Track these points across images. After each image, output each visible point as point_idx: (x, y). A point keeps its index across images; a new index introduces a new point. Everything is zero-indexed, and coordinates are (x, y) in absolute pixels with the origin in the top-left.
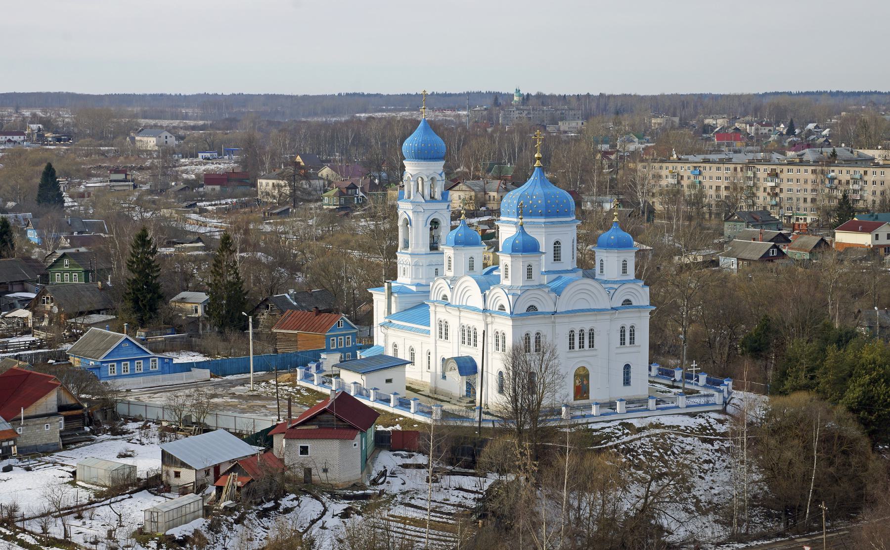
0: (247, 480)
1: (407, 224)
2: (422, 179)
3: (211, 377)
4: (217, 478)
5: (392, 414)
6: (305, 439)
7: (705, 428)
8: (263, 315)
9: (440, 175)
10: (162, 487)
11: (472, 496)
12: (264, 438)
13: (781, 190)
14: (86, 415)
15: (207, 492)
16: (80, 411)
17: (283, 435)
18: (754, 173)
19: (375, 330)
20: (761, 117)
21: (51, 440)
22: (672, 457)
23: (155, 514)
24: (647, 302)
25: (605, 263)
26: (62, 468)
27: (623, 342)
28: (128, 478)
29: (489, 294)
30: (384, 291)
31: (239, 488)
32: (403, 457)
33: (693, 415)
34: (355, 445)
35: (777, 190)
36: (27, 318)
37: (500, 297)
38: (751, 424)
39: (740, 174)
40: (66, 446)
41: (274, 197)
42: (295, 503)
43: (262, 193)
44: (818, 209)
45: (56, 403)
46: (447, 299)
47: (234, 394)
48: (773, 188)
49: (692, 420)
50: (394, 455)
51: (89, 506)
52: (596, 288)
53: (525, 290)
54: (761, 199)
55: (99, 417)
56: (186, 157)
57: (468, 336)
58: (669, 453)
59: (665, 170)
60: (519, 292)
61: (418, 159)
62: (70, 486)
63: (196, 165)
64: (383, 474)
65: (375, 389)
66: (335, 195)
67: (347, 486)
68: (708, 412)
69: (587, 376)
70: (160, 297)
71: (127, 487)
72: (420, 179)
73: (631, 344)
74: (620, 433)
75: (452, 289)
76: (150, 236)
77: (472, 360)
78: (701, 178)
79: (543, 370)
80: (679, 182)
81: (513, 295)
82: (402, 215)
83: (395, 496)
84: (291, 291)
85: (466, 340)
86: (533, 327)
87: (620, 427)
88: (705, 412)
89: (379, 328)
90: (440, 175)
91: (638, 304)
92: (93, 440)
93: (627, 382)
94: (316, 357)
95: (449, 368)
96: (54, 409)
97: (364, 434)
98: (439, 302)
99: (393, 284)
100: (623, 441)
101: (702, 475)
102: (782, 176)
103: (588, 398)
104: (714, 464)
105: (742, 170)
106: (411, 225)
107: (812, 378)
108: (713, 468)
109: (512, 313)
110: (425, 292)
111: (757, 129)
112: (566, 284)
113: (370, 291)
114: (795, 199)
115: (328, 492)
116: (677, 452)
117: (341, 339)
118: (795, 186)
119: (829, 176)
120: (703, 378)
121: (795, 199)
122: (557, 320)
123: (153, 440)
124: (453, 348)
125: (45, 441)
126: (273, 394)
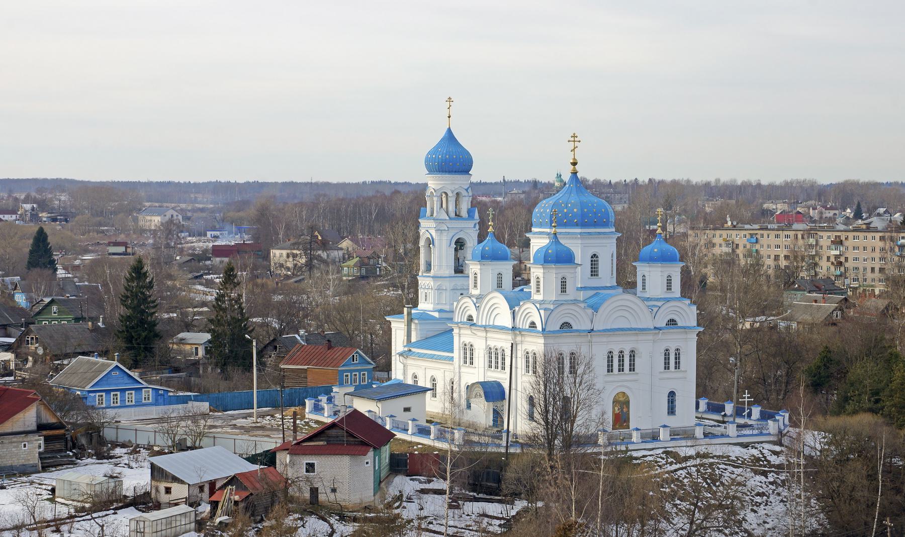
0: (245, 494)
1: (430, 244)
2: (446, 193)
3: (211, 411)
4: (212, 492)
5: (411, 442)
6: (312, 454)
7: (758, 460)
8: (270, 357)
9: (467, 190)
10: (150, 505)
11: (498, 522)
12: (269, 458)
13: (846, 259)
14: (69, 439)
15: (200, 509)
16: (62, 431)
17: (287, 452)
18: (817, 241)
19: (393, 358)
20: (825, 202)
21: (29, 460)
22: (721, 488)
23: (142, 524)
24: (694, 323)
25: (647, 278)
26: (40, 486)
27: (667, 367)
28: (112, 493)
29: (519, 310)
30: (403, 318)
31: (236, 503)
32: (421, 482)
33: (745, 446)
34: (367, 463)
35: (842, 259)
36: (9, 361)
37: (532, 313)
38: (809, 458)
39: (800, 242)
40: (45, 468)
41: (288, 269)
42: (300, 523)
43: (275, 264)
44: (887, 279)
45: (35, 419)
46: (472, 320)
47: (235, 425)
48: (837, 257)
49: (744, 450)
50: (411, 480)
51: (68, 521)
52: (636, 304)
53: (558, 304)
54: (825, 268)
55: (83, 441)
56: (194, 236)
57: (495, 358)
58: (717, 484)
59: (719, 237)
60: (552, 307)
61: (442, 172)
62: (47, 502)
63: (204, 242)
64: (399, 498)
65: (392, 416)
66: (355, 265)
67: (358, 508)
68: (762, 442)
69: (627, 403)
70: (157, 335)
71: (112, 503)
72: (444, 195)
73: (676, 368)
74: (664, 462)
75: (477, 308)
76: (145, 269)
77: (499, 385)
78: (758, 247)
79: (577, 385)
80: (733, 251)
81: (545, 310)
82: (424, 233)
83: (412, 521)
84: (302, 332)
85: (493, 364)
86: (566, 345)
87: (664, 456)
88: (758, 443)
89: (398, 356)
90: (467, 190)
91: (684, 325)
92: (76, 464)
93: (671, 411)
94: (328, 391)
95: (474, 393)
96: (33, 427)
97: (378, 451)
98: (464, 323)
99: (413, 311)
100: (666, 470)
101: (755, 508)
102: (846, 243)
103: (629, 428)
104: (768, 497)
105: (803, 238)
106: (433, 245)
107: (877, 401)
108: (767, 501)
109: (543, 330)
110: (447, 315)
111: (821, 213)
112: (604, 300)
113: (388, 318)
114: (861, 269)
115: (336, 514)
116: (727, 483)
117: (356, 375)
118: (862, 255)
119: (899, 243)
120: (756, 411)
121: (861, 269)
122: (594, 339)
123: (142, 464)
124: (477, 373)
125: (22, 462)
126: (279, 426)
